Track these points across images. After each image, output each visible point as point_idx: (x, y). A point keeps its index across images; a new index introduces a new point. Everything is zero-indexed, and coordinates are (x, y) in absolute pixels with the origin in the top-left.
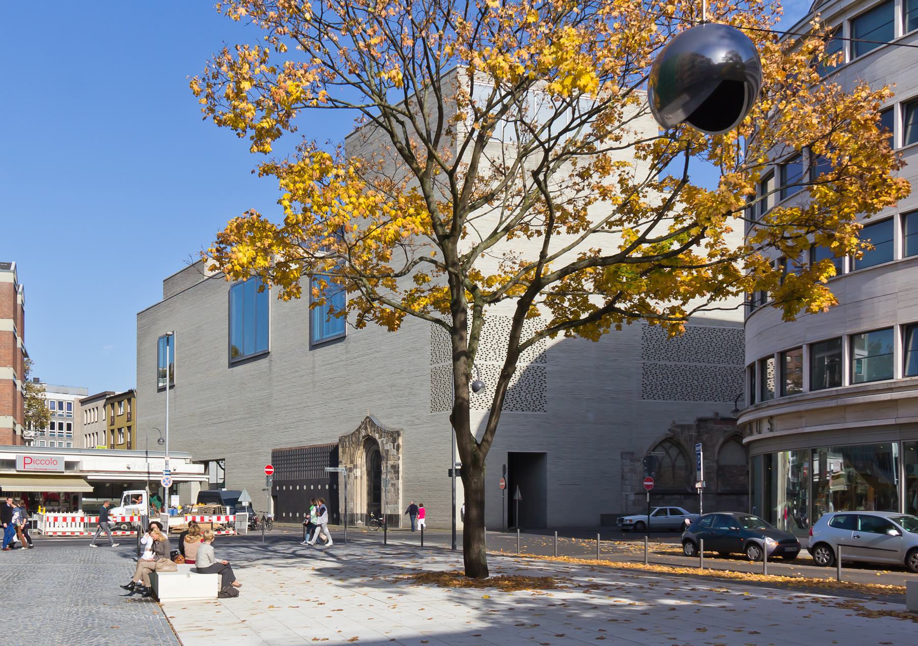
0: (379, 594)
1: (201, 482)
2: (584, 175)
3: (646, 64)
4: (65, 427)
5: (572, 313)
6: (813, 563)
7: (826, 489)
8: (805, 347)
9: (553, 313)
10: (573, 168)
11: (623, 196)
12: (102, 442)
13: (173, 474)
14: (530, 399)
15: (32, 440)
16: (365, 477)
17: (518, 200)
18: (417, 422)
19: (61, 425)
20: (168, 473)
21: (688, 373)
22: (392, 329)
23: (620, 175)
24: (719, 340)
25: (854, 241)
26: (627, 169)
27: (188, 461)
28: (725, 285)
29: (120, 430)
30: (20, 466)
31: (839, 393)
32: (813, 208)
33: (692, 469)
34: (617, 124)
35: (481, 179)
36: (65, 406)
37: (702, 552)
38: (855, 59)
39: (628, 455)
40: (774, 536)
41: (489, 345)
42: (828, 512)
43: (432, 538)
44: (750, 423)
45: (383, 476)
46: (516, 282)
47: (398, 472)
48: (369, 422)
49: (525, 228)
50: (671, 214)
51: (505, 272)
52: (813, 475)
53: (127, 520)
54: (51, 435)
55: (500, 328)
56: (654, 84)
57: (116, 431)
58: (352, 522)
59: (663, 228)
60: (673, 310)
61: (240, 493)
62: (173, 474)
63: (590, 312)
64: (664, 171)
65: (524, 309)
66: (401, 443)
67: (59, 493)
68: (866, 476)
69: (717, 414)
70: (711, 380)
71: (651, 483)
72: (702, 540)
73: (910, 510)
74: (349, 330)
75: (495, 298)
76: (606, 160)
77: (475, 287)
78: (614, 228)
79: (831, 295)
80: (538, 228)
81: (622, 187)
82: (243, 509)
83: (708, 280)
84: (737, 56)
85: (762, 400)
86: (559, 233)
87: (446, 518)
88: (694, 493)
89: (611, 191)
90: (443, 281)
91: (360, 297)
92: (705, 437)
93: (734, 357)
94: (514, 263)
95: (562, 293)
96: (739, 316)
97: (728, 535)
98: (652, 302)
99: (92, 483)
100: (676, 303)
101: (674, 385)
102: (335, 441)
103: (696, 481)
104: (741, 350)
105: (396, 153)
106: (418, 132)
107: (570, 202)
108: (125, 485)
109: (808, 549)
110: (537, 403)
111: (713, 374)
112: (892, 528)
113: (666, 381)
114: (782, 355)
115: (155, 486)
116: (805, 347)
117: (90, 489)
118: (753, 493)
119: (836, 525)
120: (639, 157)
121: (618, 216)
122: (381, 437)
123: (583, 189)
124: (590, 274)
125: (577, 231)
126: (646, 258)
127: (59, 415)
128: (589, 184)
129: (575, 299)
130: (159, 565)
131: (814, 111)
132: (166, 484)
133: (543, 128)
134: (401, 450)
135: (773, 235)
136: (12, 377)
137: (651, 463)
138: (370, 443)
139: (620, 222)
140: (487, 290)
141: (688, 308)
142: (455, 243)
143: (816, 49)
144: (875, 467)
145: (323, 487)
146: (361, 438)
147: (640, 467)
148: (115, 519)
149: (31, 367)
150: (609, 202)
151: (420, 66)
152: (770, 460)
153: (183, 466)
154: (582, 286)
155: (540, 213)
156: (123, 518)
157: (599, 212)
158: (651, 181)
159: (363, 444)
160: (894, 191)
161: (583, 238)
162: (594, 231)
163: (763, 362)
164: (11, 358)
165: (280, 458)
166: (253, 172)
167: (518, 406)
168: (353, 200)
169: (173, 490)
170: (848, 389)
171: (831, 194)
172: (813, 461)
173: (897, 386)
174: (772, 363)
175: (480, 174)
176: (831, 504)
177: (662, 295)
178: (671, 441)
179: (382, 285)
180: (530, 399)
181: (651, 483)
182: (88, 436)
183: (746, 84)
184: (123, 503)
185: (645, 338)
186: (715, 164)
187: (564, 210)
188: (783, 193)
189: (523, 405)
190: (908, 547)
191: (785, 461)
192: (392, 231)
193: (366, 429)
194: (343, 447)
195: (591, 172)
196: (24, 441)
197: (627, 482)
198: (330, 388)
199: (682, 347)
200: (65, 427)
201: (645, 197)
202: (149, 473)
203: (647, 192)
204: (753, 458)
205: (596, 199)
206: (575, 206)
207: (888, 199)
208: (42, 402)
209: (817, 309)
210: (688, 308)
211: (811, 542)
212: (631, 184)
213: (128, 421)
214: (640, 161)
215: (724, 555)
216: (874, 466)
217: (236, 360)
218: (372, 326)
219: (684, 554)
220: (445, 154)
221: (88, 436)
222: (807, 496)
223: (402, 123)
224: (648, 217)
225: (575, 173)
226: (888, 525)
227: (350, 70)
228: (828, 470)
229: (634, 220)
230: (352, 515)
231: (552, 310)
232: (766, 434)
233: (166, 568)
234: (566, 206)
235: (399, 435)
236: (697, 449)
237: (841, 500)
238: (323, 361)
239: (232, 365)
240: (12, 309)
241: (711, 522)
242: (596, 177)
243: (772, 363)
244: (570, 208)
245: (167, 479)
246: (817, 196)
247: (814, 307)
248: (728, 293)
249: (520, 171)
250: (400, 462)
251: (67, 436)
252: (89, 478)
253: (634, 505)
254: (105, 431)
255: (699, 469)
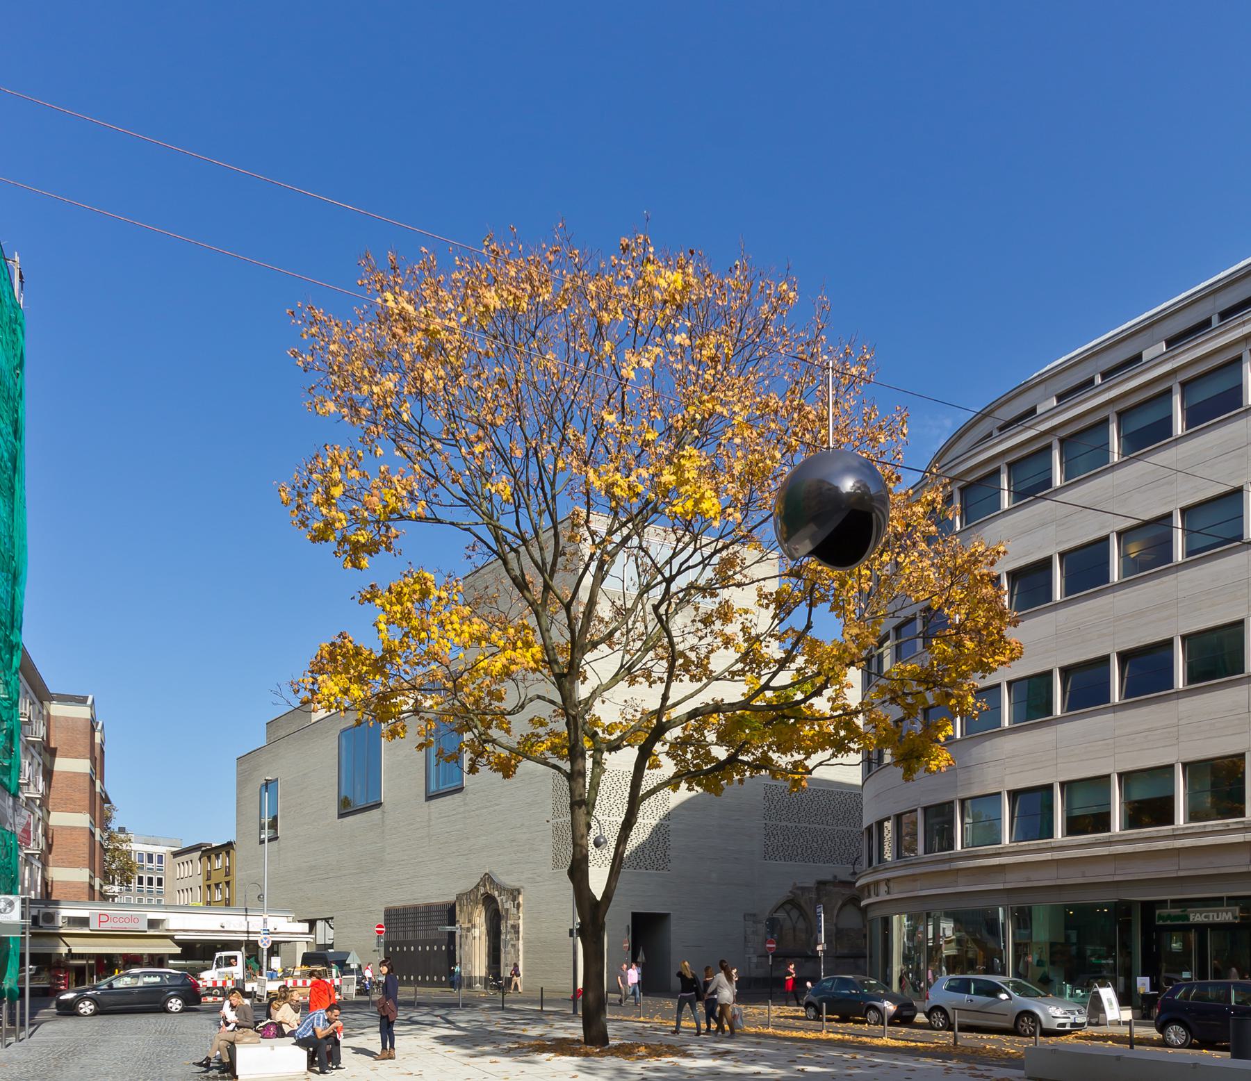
0: (505, 1062)
1: (307, 942)
2: (707, 621)
3: (769, 497)
4: (155, 882)
5: (695, 766)
6: (930, 1027)
7: (939, 953)
8: (919, 810)
9: (676, 764)
10: (695, 613)
11: (746, 645)
12: (197, 898)
13: (272, 933)
14: (653, 858)
15: (117, 896)
16: (484, 937)
17: (638, 644)
18: (538, 879)
19: (150, 881)
20: (267, 932)
21: (808, 835)
22: (507, 776)
23: (742, 623)
24: (837, 802)
25: (971, 699)
26: (749, 616)
27: (290, 919)
28: (846, 741)
29: (217, 885)
30: (94, 925)
31: (952, 857)
32: (933, 664)
33: (812, 932)
34: (738, 569)
35: (601, 620)
36: (155, 859)
37: (825, 1016)
38: (964, 527)
39: (751, 917)
40: (892, 999)
41: (612, 800)
42: (941, 975)
43: (552, 1002)
44: (868, 885)
45: (503, 937)
46: (636, 730)
47: (517, 932)
48: (488, 879)
49: (648, 674)
50: (793, 666)
51: (626, 720)
52: (928, 940)
53: (220, 984)
54: (138, 891)
55: (623, 783)
56: (780, 512)
57: (213, 887)
58: (470, 986)
59: (784, 678)
60: (796, 765)
61: (348, 954)
62: (272, 933)
63: (713, 765)
64: (788, 619)
65: (645, 753)
66: (521, 902)
67: (142, 955)
68: (975, 941)
69: (835, 877)
70: (829, 843)
71: (774, 946)
72: (824, 1004)
73: (1017, 973)
74: (467, 779)
75: (615, 747)
76: (728, 607)
77: (596, 733)
78: (736, 678)
79: (948, 755)
80: (660, 675)
81: (744, 635)
82: (351, 972)
83: (830, 735)
84: (865, 486)
85: (879, 863)
86: (681, 681)
87: (568, 981)
88: (815, 956)
89: (734, 640)
90: (561, 726)
91: (472, 739)
92: (824, 899)
93: (851, 821)
94: (636, 711)
95: (683, 743)
96: (858, 781)
97: (848, 999)
98: (774, 756)
99: (179, 943)
100: (798, 757)
101: (795, 847)
102: (452, 898)
103: (817, 943)
104: (857, 814)
105: (508, 582)
106: (532, 558)
107: (692, 649)
108: (219, 946)
109: (925, 1013)
110: (660, 861)
111: (831, 837)
112: (1002, 992)
113: (787, 843)
114: (899, 818)
115: (252, 949)
116: (919, 810)
117: (178, 950)
118: (871, 956)
119: (950, 988)
120: (761, 605)
121: (740, 666)
122: (500, 895)
123: (706, 636)
124: (713, 724)
125: (700, 680)
126: (770, 707)
127: (148, 869)
128: (712, 632)
129: (697, 751)
130: (239, 1036)
131: (932, 565)
132: (264, 945)
133: (666, 563)
134: (521, 909)
135: (893, 691)
136: (87, 825)
137: (773, 924)
138: (489, 901)
139: (742, 672)
140: (608, 737)
141: (810, 763)
142: (572, 683)
143: (934, 501)
144: (985, 933)
145: (439, 948)
146: (479, 896)
147: (762, 928)
148: (205, 984)
149: (115, 814)
150: (732, 650)
151: (535, 490)
152: (887, 923)
153: (285, 925)
154: (705, 737)
155: (662, 659)
156: (215, 983)
157: (722, 660)
158: (773, 630)
159: (481, 902)
160: (1008, 652)
161: (706, 685)
162: (717, 679)
163: (880, 824)
164: (87, 803)
165: (393, 916)
166: (353, 598)
167: (642, 864)
168: (457, 626)
169: (274, 950)
170: (960, 853)
171: (950, 650)
172: (928, 925)
173: (1005, 851)
174: (888, 825)
175: (601, 615)
176: (944, 969)
177: (783, 749)
178: (792, 903)
179: (496, 727)
180: (653, 858)
181: (774, 946)
182: (181, 892)
183: (874, 515)
184: (215, 966)
185: (767, 798)
186: (838, 617)
187: (686, 657)
188: (898, 656)
189: (647, 863)
190: (1018, 1011)
191: (900, 925)
192: (499, 665)
193: (485, 886)
194: (460, 905)
195: (714, 619)
196: (104, 897)
197: (749, 945)
198: (446, 843)
199: (802, 809)
200: (155, 882)
201: (767, 647)
202: (248, 932)
203: (769, 642)
204: (871, 921)
205: (718, 648)
206: (697, 653)
207: (1003, 659)
208: (129, 853)
209: (934, 768)
210: (810, 763)
211: (927, 1006)
212: (753, 633)
213: (226, 876)
214: (763, 610)
215: (844, 1019)
216: (983, 931)
217: (346, 809)
218: (484, 772)
219: (806, 1018)
220: (562, 584)
221: (181, 892)
222: (922, 960)
223: (516, 551)
224: (770, 668)
225: (697, 619)
226: (1000, 990)
227: (453, 479)
228: (941, 934)
229: (756, 670)
230: (470, 978)
231: (675, 762)
232: (883, 897)
233: (247, 1040)
234: (688, 653)
235: (519, 893)
236: (818, 910)
237: (953, 964)
238: (440, 814)
239: (341, 816)
240: (88, 748)
241: (833, 985)
242: (718, 625)
243: (888, 825)
244: (692, 656)
245: (265, 938)
246: (936, 651)
247: (933, 766)
248: (850, 749)
249: (642, 614)
250: (521, 922)
251: (127, 890)
252: (176, 937)
253: (757, 967)
254: (200, 887)
255: (820, 932)
